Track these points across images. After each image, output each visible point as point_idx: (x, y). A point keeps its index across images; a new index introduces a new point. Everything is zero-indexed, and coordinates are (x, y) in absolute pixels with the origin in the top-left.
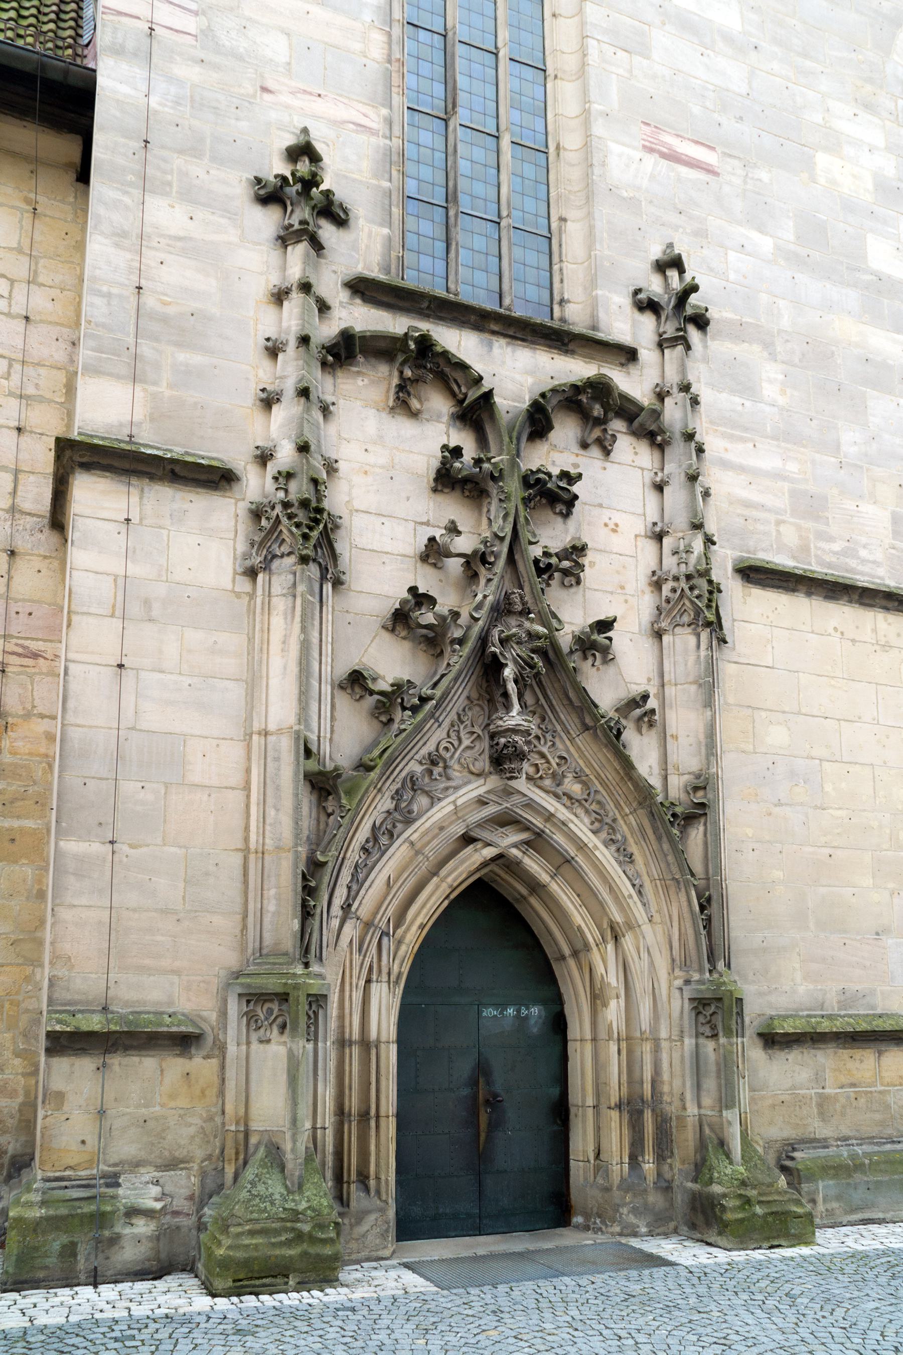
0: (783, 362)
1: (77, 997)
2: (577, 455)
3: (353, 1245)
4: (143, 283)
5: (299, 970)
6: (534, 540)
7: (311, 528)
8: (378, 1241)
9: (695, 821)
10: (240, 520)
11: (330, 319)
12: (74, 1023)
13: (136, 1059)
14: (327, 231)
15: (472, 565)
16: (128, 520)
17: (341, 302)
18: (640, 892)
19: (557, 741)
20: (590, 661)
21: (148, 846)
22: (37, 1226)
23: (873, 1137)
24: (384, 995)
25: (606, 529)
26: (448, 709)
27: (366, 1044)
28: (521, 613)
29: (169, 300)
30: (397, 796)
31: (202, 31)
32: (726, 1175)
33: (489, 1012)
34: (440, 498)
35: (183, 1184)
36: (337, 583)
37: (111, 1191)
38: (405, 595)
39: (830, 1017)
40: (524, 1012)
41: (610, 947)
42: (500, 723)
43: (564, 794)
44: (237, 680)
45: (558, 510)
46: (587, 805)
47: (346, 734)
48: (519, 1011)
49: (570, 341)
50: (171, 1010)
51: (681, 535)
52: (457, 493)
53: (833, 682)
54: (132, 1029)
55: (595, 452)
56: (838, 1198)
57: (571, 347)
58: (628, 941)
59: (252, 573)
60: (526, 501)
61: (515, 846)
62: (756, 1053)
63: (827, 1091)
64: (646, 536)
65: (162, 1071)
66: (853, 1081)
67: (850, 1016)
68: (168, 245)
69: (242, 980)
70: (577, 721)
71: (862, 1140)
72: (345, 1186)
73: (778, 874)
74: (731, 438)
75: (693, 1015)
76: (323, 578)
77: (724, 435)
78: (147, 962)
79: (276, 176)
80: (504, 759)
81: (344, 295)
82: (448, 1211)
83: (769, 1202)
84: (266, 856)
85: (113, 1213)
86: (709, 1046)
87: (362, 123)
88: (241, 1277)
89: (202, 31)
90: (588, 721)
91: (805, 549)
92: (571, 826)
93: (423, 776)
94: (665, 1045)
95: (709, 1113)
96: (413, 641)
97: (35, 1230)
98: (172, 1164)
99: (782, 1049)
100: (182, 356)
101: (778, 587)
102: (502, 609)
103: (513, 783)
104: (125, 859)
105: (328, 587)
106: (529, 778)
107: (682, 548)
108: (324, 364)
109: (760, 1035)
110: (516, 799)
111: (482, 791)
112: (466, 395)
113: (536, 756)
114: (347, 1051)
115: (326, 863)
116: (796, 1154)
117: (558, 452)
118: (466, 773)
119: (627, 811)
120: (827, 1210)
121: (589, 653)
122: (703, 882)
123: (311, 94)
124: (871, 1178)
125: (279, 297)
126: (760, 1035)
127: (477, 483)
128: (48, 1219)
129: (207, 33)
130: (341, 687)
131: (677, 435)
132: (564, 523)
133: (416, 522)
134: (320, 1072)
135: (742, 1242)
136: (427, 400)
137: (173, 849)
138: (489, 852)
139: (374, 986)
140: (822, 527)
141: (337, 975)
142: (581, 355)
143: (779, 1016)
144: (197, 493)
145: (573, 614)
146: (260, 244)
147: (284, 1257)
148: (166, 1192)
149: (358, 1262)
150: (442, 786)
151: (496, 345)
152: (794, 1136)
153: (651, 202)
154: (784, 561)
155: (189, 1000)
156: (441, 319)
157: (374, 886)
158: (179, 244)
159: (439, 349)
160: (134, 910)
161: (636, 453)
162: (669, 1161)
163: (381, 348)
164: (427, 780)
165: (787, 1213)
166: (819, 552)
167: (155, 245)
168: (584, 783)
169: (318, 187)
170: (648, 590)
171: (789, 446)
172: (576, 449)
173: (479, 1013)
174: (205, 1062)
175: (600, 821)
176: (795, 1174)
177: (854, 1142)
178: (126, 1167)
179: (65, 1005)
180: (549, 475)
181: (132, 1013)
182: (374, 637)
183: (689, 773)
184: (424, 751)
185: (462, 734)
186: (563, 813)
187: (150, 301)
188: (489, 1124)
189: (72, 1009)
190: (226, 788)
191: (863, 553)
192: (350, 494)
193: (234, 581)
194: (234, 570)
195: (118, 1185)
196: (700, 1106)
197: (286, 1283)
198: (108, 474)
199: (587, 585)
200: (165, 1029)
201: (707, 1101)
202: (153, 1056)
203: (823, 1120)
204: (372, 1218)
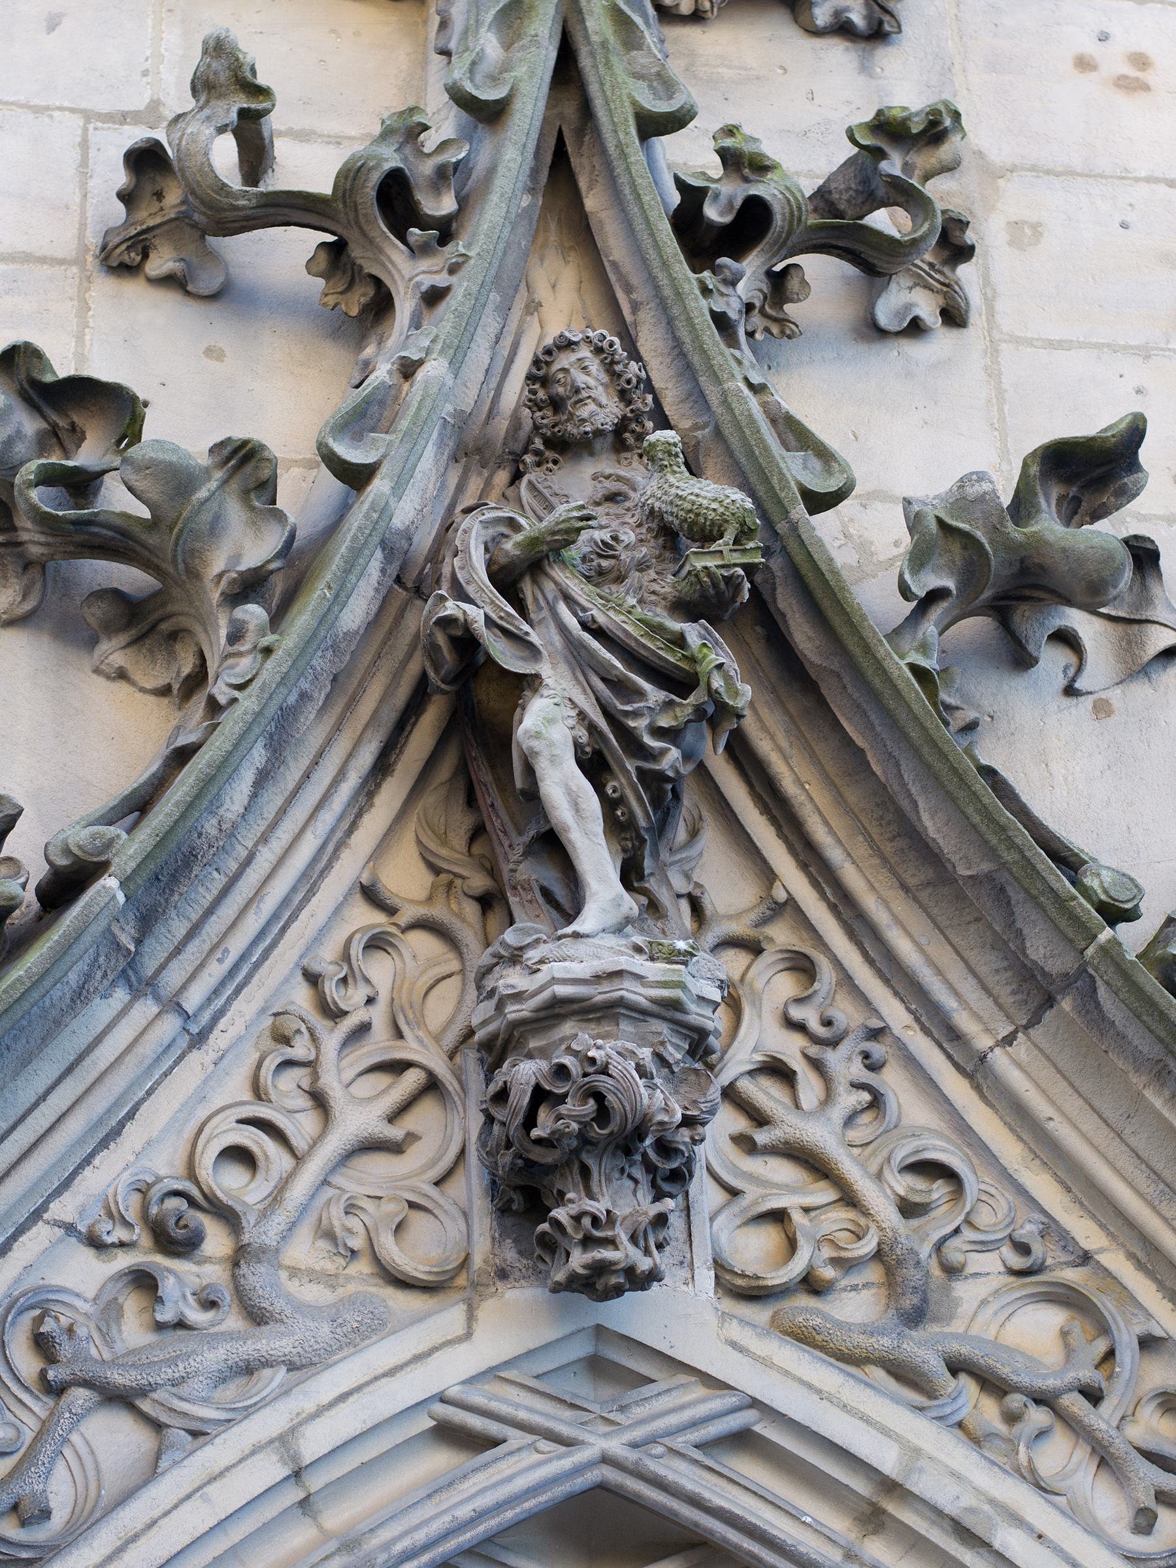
15: (356, 252)
19: (894, 1081)
25: (1088, 83)
28: (622, 438)
43: (955, 1367)
46: (1102, 1419)
70: (987, 962)
80: (560, 1171)
90: (1041, 948)
93: (110, 1312)
103: (632, 1315)
110: (669, 1406)
111: (450, 1371)
113: (782, 1171)
121: (1036, 628)
132: (865, 68)
133: (88, 116)
150: (214, 1357)
164: (133, 1331)
168: (1067, 1298)
185: (331, 1082)
199: (1007, 322)
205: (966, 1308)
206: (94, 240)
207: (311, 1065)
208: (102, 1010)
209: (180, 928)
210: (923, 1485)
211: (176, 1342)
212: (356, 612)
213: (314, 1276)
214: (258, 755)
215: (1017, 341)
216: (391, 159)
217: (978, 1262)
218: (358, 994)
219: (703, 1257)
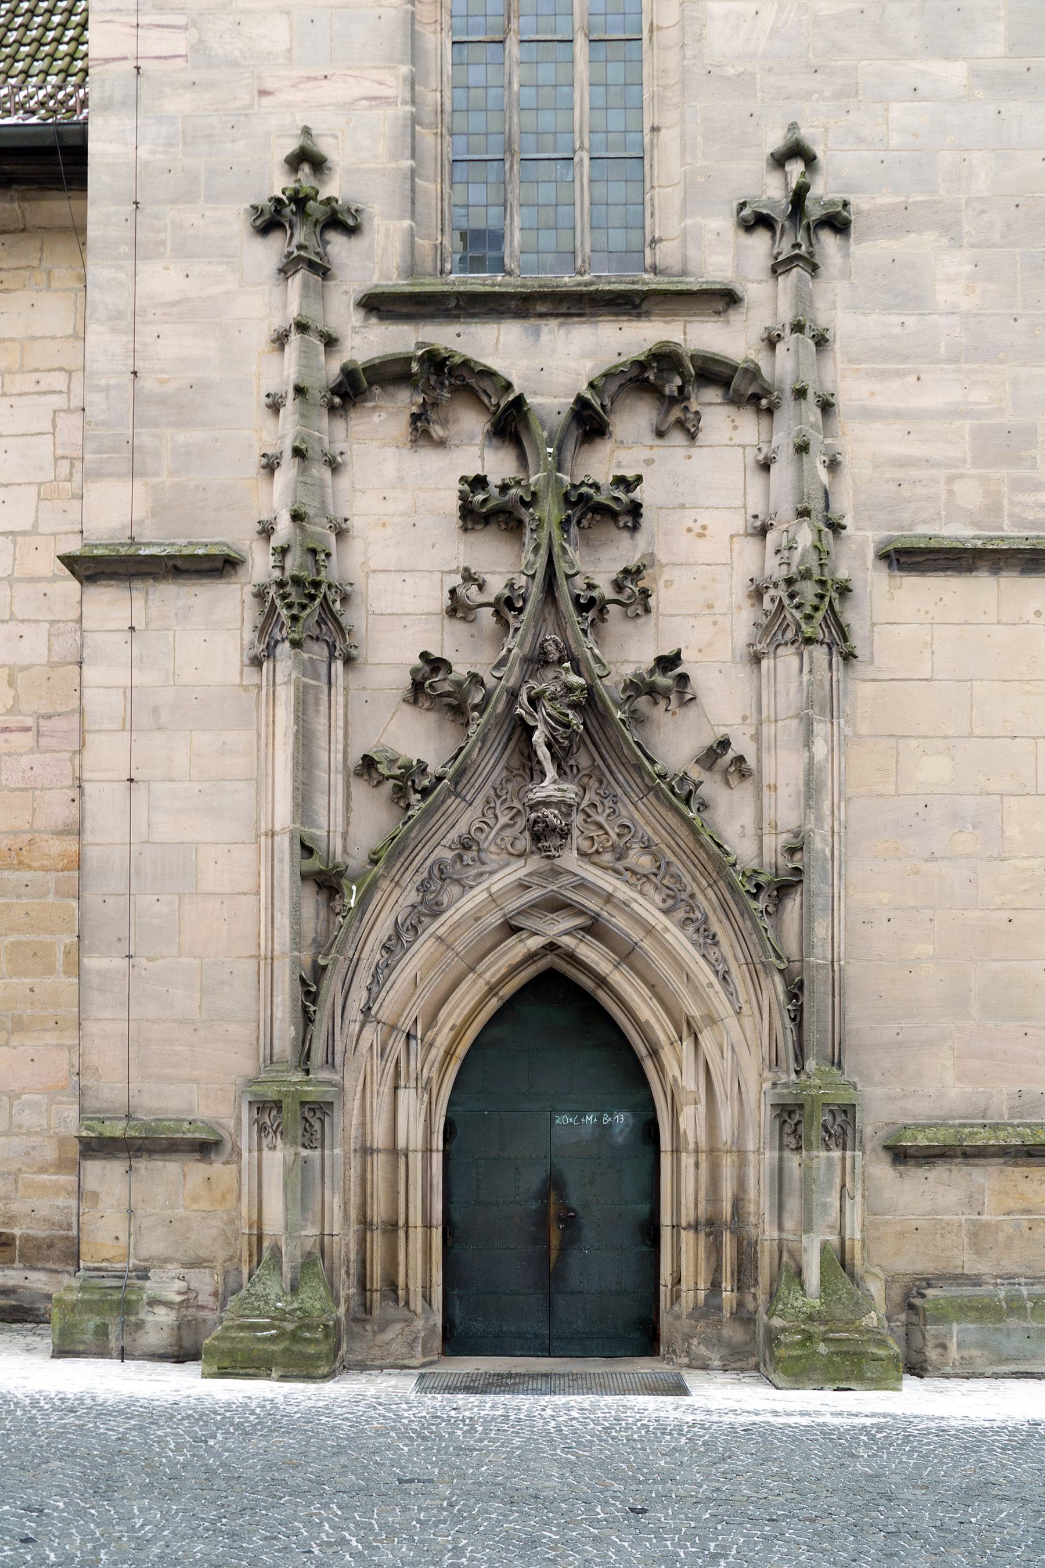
0: (972, 246)
1: (105, 1105)
2: (651, 448)
3: (376, 1351)
4: (140, 365)
5: (298, 1076)
6: (572, 572)
7: (304, 607)
8: (404, 1350)
9: (793, 890)
10: (247, 605)
11: (341, 351)
12: (100, 1130)
13: (160, 1164)
14: (338, 244)
16: (132, 628)
17: (353, 328)
20: (663, 704)
21: (164, 958)
22: (74, 1306)
24: (412, 1101)
26: (477, 785)
27: (393, 1151)
29: (167, 376)
30: (423, 887)
31: (192, 47)
32: (793, 1307)
33: (563, 1119)
34: (472, 537)
35: (205, 1282)
36: (349, 661)
37: (139, 1283)
38: (418, 662)
39: (995, 1127)
40: (606, 1119)
41: (687, 1045)
42: (531, 795)
44: (247, 780)
45: (621, 524)
47: (358, 825)
48: (600, 1118)
50: (191, 1118)
51: (784, 526)
52: (493, 528)
53: (1028, 687)
54: (150, 1135)
55: (677, 438)
56: (982, 1345)
57: (645, 307)
58: (707, 1038)
59: (257, 662)
60: (565, 525)
61: (567, 933)
62: (883, 1170)
63: (985, 1217)
64: (747, 535)
65: (184, 1175)
66: (1027, 1205)
67: (1028, 1126)
68: (165, 314)
69: (255, 1088)
72: (368, 1293)
73: (925, 948)
74: (882, 375)
75: (777, 1123)
76: (332, 657)
77: (869, 375)
78: (167, 1071)
79: (270, 200)
80: (544, 835)
81: (357, 317)
82: (513, 1329)
83: (839, 1340)
84: (275, 961)
85: (138, 1301)
86: (794, 1161)
87: (377, 94)
88: (225, 1365)
89: (192, 47)
91: (994, 509)
92: (635, 906)
94: (752, 1158)
95: (791, 1237)
96: (439, 711)
97: (72, 1310)
98: (196, 1263)
99: (919, 1165)
100: (182, 437)
102: (538, 660)
104: (143, 973)
105: (338, 666)
106: (582, 854)
107: (784, 543)
108: (332, 409)
109: (887, 1148)
110: (565, 880)
111: (521, 873)
112: (498, 405)
113: (593, 827)
114: (369, 1159)
115: (326, 966)
116: (930, 1292)
117: (631, 447)
118: (504, 856)
119: (705, 883)
122: (797, 964)
123: (315, 79)
125: (281, 340)
126: (887, 1148)
127: (511, 513)
128: (82, 1302)
129: (199, 47)
130: (358, 775)
131: (788, 394)
132: (632, 538)
133: (443, 572)
134: (327, 1180)
135: (797, 1382)
136: (456, 421)
137: (188, 960)
138: (534, 943)
139: (401, 1092)
140: (1023, 473)
141: (357, 1081)
142: (658, 315)
143: (917, 1125)
145: (628, 652)
146: (261, 284)
147: (266, 1351)
148: (191, 1287)
149: (381, 1368)
150: (474, 872)
151: (545, 330)
152: (931, 1270)
153: (770, 70)
154: (957, 531)
155: (208, 1108)
156: (473, 316)
157: (396, 987)
158: (174, 310)
159: (457, 360)
160: (154, 1022)
161: (735, 428)
162: (752, 1290)
163: (389, 374)
164: (458, 866)
166: (1017, 510)
167: (150, 317)
169: (315, 199)
170: (746, 603)
171: (976, 366)
172: (650, 439)
173: (552, 1120)
174: (224, 1167)
175: (674, 897)
176: (921, 1314)
177: (1023, 1280)
178: (155, 1263)
179: (95, 1112)
180: (596, 486)
181: (156, 1120)
182: (394, 714)
183: (788, 831)
184: (453, 835)
185: (498, 812)
186: (622, 890)
187: (147, 383)
188: (562, 1242)
189: (102, 1116)
190: (239, 894)
192: (365, 554)
193: (241, 674)
194: (242, 661)
195: (148, 1278)
196: (781, 1228)
198: (113, 582)
199: (661, 610)
200: (180, 1135)
201: (789, 1224)
202: (176, 1161)
203: (977, 1252)
204: (398, 1327)
205: (631, 855)
206: (444, 608)
207: (494, 808)
208: (449, 801)
209: (465, 782)
210: (618, 895)
211: (469, 869)
212: (500, 708)
213: (496, 853)
214: (479, 744)
215: (664, 615)
216: (507, 593)
217: (634, 846)
218: (504, 792)
219: (574, 847)
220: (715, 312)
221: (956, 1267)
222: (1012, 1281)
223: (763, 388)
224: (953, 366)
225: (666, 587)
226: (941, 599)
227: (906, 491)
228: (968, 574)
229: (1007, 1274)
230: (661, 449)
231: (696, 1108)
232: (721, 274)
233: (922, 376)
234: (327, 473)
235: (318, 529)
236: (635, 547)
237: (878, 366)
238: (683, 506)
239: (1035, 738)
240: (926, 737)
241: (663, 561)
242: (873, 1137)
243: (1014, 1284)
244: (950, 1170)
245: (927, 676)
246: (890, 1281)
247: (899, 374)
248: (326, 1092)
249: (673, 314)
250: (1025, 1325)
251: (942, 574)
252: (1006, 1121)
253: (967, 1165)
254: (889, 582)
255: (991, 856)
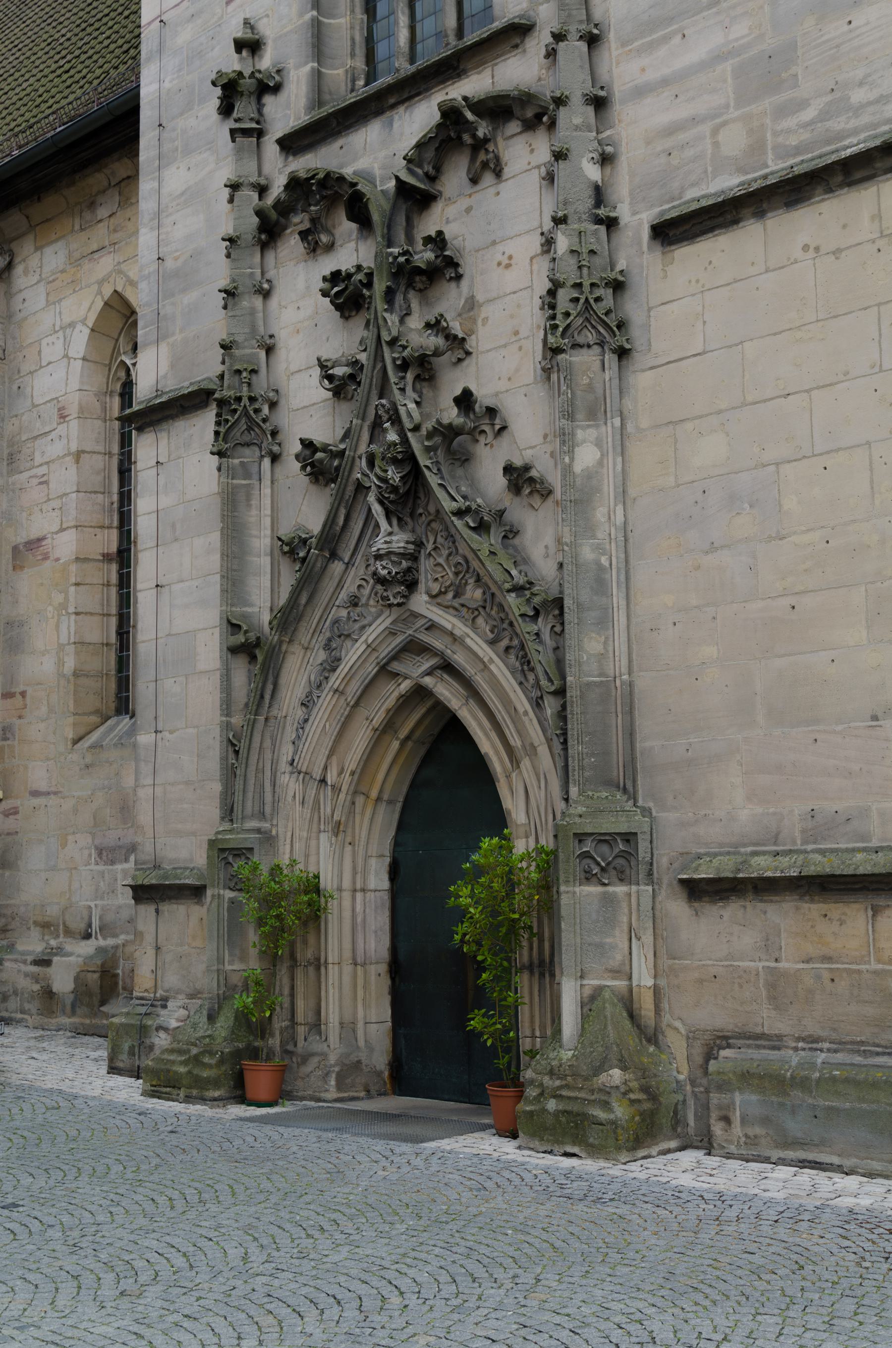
13: (175, 906)
18: (538, 705)
23: (862, 1043)
49: (459, 61)
50: (192, 866)
56: (765, 1121)
63: (782, 965)
71: (840, 1045)
73: (710, 651)
74: (651, 47)
77: (639, 51)
92: (468, 641)
99: (713, 902)
101: (711, 229)
105: (267, 462)
120: (746, 1136)
124: (821, 1102)
144: (197, 416)
152: (731, 1027)
159: (321, 175)
165: (585, 1116)
166: (780, 139)
172: (468, 189)
184: (343, 595)
191: (858, 96)
197: (178, 1095)
199: (480, 349)
202: (183, 904)
220: (513, 47)
221: (756, 1025)
222: (814, 1046)
223: (541, 107)
224: (714, 10)
225: (483, 325)
226: (710, 263)
227: (675, 161)
228: (735, 227)
229: (810, 1036)
230: (477, 194)
231: (527, 841)
232: (519, 7)
233: (685, 32)
234: (258, 301)
235: (248, 351)
236: (460, 295)
237: (649, 39)
238: (494, 243)
239: (807, 391)
240: (701, 417)
241: (481, 301)
242: (669, 869)
243: (816, 1049)
244: (745, 907)
245: (699, 351)
246: (690, 1038)
247: (666, 39)
248: (245, 839)
249: (482, 63)
250: (810, 1101)
251: (710, 235)
252: (799, 847)
253: (761, 901)
254: (662, 260)
255: (770, 537)
